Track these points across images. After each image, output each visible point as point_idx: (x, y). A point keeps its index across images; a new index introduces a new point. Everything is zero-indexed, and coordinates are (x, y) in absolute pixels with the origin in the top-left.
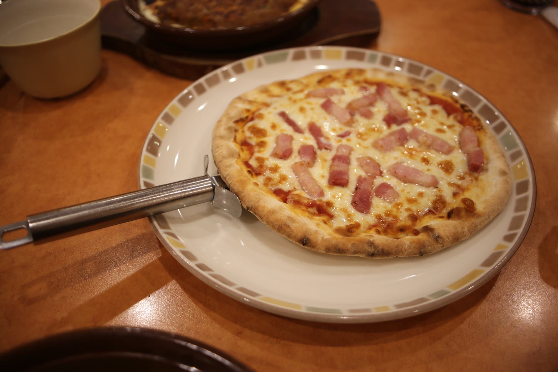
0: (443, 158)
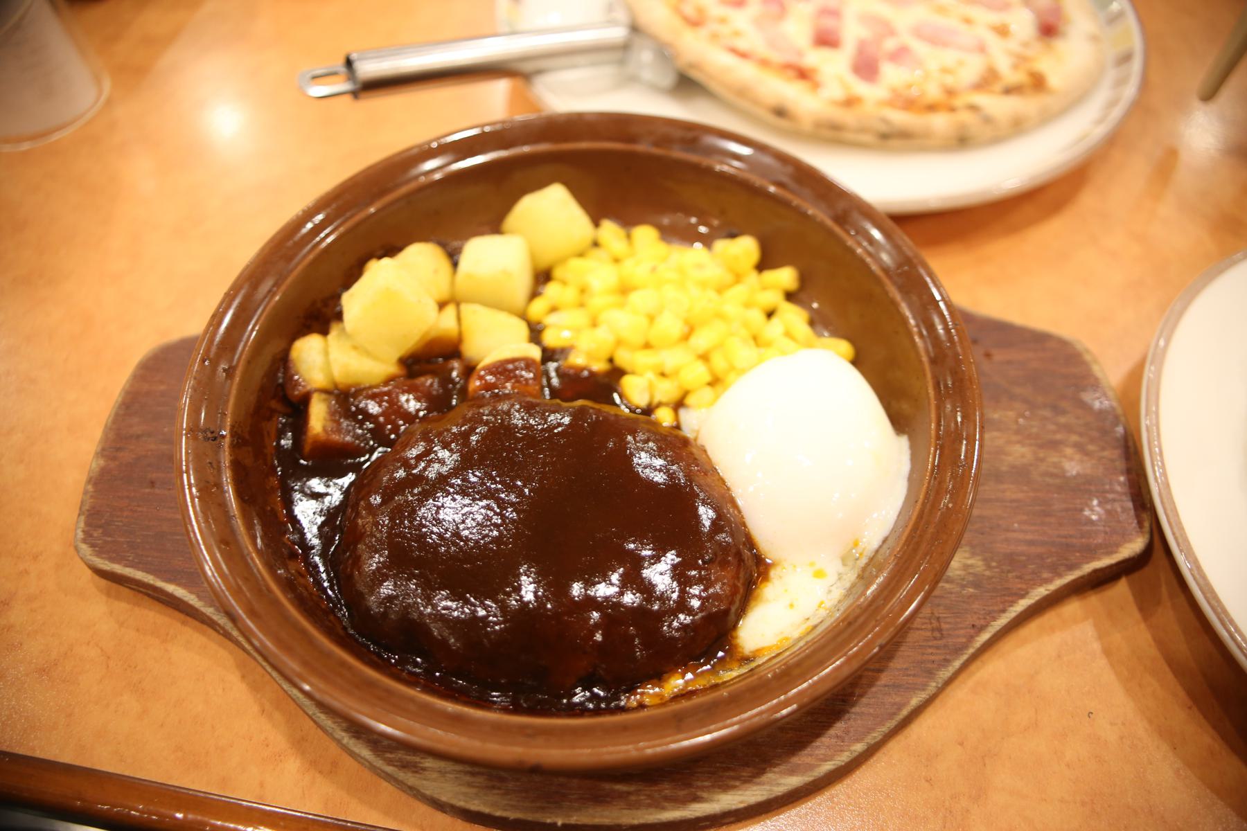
0: (994, 18)
